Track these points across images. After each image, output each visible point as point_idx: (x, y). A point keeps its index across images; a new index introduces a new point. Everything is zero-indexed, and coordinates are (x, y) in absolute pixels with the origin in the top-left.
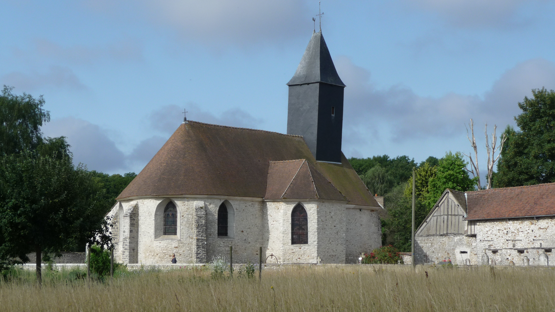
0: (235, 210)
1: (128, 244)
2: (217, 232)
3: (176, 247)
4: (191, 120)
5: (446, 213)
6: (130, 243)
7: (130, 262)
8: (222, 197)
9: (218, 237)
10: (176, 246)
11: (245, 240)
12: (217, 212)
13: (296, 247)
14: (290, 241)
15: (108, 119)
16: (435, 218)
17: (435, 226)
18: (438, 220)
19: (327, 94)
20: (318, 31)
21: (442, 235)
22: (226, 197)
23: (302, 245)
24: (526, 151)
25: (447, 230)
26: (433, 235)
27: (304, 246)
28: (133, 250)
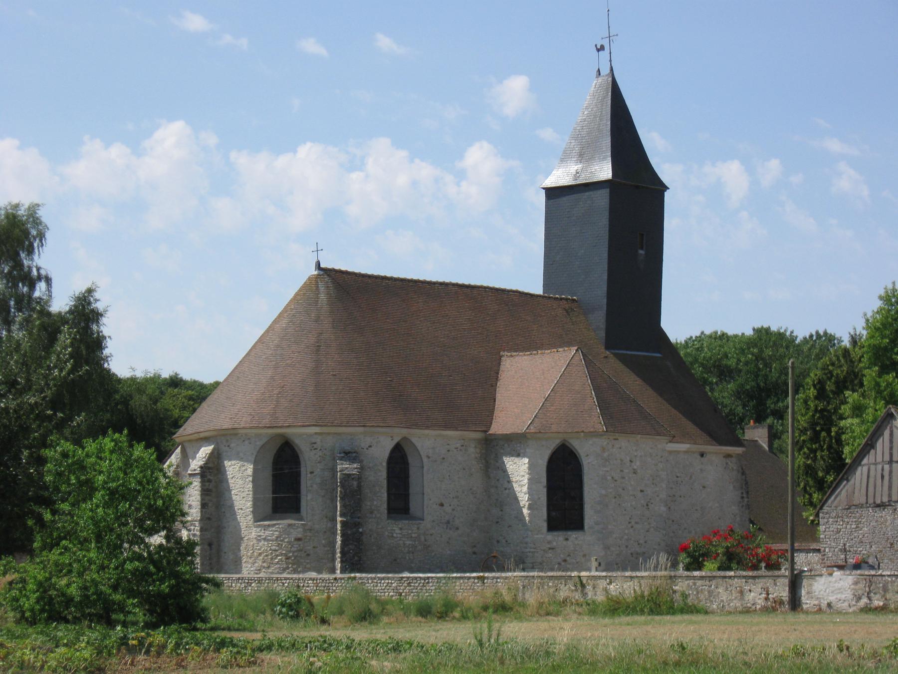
0: (425, 460)
1: (198, 533)
2: (385, 506)
3: (299, 539)
4: (330, 266)
5: (887, 458)
6: (201, 530)
7: (554, 525)
8: (396, 430)
9: (389, 518)
10: (300, 536)
11: (448, 522)
12: (385, 464)
13: (558, 538)
14: (545, 525)
15: (183, 284)
16: (865, 469)
17: (864, 485)
18: (872, 473)
19: (620, 216)
20: (605, 71)
21: (878, 506)
22: (405, 432)
23: (569, 533)
24: (183, 664)
25: (890, 495)
26: (861, 506)
27: (573, 535)
28: (210, 545)
